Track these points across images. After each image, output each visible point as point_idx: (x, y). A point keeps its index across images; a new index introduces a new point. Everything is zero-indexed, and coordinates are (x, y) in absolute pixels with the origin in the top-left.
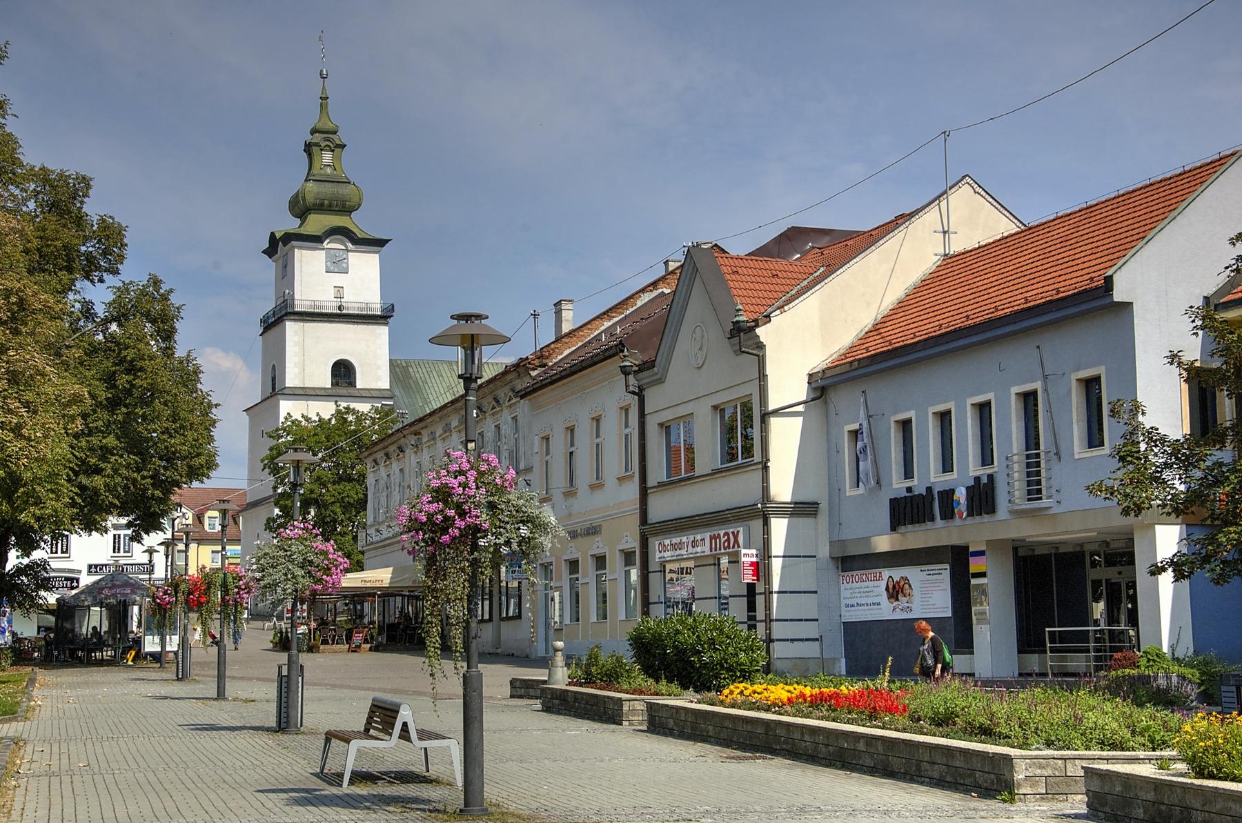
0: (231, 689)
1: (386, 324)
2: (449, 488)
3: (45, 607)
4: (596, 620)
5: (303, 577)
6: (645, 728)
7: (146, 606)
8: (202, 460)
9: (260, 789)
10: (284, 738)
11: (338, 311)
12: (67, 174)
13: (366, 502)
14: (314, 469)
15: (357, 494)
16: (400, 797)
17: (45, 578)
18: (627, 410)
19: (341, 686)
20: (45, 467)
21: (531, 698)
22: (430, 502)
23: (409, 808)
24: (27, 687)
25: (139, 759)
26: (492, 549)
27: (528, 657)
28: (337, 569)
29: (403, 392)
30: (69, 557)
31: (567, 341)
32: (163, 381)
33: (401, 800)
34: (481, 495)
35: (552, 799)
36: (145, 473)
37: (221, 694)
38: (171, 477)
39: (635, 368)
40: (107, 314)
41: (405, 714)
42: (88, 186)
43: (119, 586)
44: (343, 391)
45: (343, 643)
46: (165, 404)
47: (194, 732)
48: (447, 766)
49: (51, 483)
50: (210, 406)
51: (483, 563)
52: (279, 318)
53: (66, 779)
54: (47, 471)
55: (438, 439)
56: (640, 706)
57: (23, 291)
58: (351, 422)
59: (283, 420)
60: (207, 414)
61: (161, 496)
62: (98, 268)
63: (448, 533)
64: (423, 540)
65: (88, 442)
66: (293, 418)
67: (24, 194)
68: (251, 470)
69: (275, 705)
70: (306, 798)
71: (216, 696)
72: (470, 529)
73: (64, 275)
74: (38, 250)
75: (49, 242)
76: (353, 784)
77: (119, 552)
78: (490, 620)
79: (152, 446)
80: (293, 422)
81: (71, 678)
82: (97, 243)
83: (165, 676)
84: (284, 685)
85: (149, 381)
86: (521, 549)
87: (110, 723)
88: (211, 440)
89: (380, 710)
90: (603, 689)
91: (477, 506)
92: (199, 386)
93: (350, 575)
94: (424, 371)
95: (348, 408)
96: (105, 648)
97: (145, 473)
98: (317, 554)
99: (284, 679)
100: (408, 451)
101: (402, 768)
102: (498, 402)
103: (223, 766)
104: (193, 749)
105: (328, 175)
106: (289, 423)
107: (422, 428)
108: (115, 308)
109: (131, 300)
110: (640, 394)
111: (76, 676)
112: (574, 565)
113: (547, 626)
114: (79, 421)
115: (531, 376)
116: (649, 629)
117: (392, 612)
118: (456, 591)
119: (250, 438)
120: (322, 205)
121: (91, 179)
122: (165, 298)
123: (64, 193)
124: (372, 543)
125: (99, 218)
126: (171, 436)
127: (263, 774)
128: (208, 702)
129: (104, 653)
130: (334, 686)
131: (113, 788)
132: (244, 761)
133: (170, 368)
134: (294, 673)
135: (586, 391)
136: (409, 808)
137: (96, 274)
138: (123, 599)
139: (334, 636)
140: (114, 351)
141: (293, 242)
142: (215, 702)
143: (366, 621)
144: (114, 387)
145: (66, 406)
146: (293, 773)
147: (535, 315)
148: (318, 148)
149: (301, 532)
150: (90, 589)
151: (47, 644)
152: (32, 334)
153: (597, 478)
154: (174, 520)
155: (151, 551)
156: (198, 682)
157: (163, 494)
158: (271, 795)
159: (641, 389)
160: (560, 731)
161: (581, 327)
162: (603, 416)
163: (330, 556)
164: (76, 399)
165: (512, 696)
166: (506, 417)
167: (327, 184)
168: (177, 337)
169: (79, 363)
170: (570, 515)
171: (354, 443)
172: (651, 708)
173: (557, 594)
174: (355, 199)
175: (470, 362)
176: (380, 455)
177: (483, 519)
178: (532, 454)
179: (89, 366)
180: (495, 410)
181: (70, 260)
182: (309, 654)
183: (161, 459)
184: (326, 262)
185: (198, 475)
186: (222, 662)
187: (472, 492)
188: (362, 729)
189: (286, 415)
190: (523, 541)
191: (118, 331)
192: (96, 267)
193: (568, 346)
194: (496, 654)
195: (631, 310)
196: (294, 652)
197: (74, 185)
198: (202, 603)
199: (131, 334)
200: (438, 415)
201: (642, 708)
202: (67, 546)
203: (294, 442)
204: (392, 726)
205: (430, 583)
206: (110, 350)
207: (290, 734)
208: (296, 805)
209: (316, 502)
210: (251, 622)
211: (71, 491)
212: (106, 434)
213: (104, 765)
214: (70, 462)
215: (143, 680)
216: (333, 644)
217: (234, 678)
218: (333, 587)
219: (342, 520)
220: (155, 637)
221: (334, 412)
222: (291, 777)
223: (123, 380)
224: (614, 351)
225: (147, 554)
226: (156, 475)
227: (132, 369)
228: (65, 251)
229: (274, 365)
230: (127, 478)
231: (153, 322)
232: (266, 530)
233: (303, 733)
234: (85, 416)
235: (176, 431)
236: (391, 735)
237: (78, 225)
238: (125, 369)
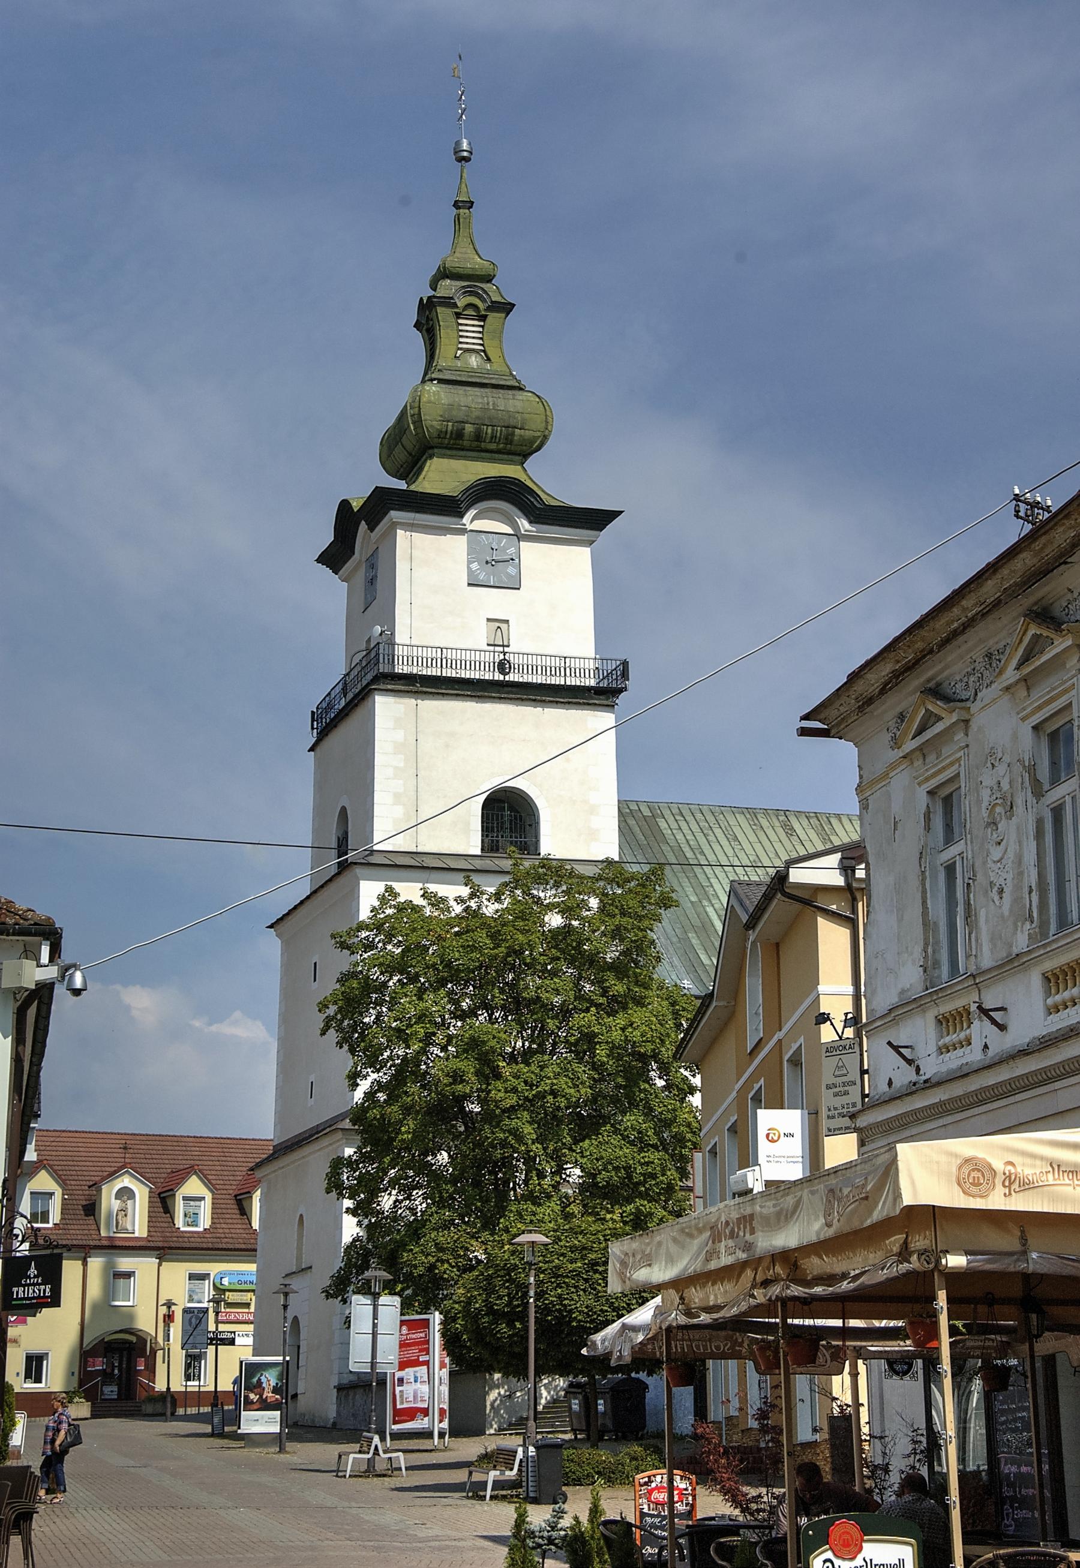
1: (610, 707)
9: (485, 1534)
66: (401, 899)
80: (401, 908)
94: (694, 827)
106: (390, 911)
120: (459, 434)
141: (393, 513)
174: (536, 424)
184: (469, 562)
210: (290, 1446)
229: (344, 810)
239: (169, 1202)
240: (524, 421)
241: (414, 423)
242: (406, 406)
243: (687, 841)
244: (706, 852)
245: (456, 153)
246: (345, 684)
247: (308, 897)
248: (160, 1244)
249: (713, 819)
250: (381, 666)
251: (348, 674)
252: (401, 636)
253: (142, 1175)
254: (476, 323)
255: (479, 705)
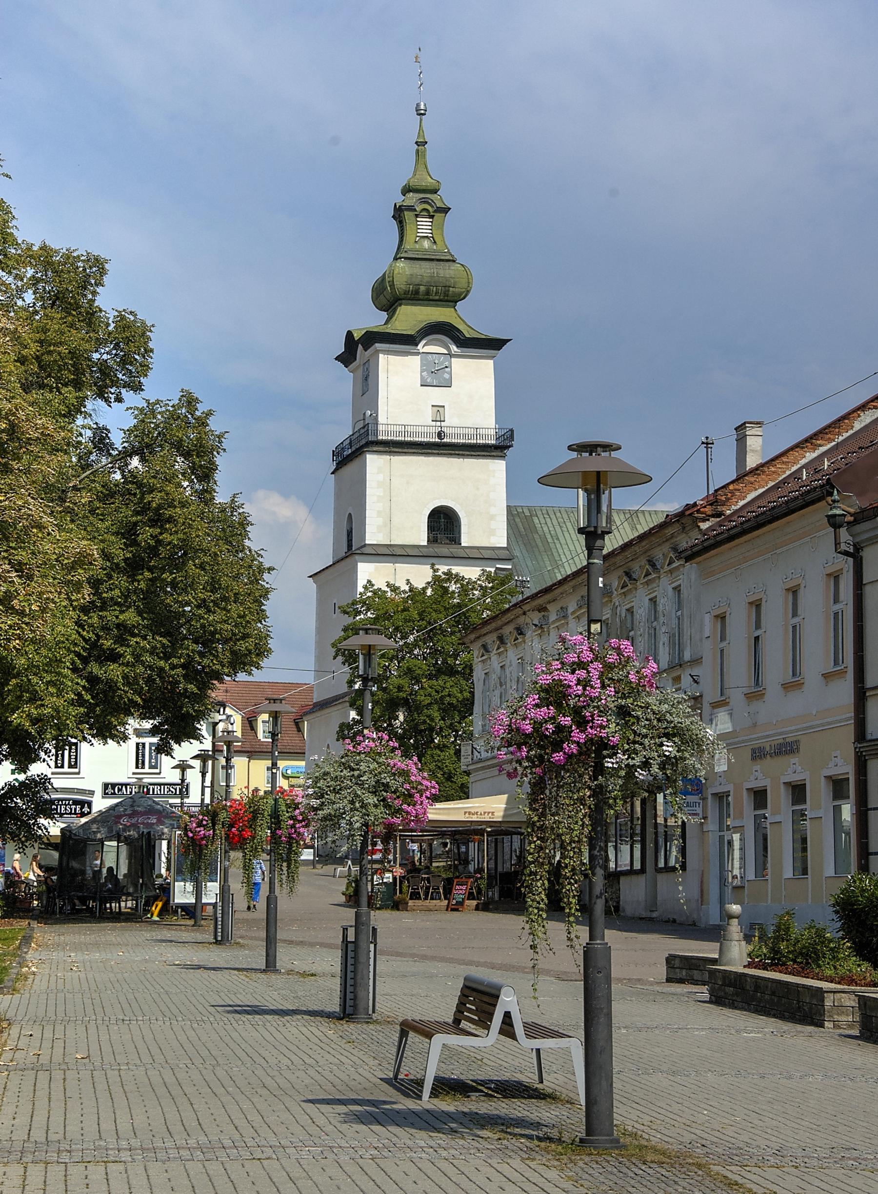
0: (284, 957)
1: (502, 457)
2: (563, 686)
3: (45, 840)
4: (791, 876)
5: (376, 806)
6: (856, 1032)
7: (176, 840)
8: (250, 644)
9: (310, 1098)
10: (350, 1028)
11: (437, 440)
12: (75, 254)
13: (473, 703)
14: (403, 658)
15: (461, 692)
16: (499, 1117)
17: (46, 800)
18: (837, 578)
19: (433, 958)
20: (44, 652)
21: (696, 983)
22: (537, 706)
23: (510, 1134)
24: (19, 948)
25: (155, 1050)
26: (623, 773)
27: (694, 924)
28: (421, 796)
29: (524, 551)
30: (79, 773)
31: (752, 479)
32: (198, 536)
33: (500, 1121)
34: (609, 697)
35: (713, 1130)
36: (175, 661)
37: (271, 965)
38: (209, 666)
39: (849, 518)
40: (126, 445)
41: (508, 1001)
42: (103, 272)
43: (142, 814)
44: (444, 550)
45: (440, 899)
46: (202, 567)
47: (230, 1016)
48: (569, 1076)
49: (51, 672)
50: (261, 570)
51: (610, 792)
52: (357, 450)
53: (58, 1075)
54: (45, 657)
55: (571, 617)
56: (850, 1001)
57: (14, 414)
58: (453, 592)
59: (362, 590)
60: (257, 580)
61: (195, 690)
62: (115, 383)
63: (562, 749)
64: (528, 758)
65: (101, 618)
66: (375, 587)
67: (20, 283)
68: (319, 658)
69: (338, 981)
70: (370, 1114)
71: (264, 967)
72: (592, 744)
73: (70, 393)
74: (37, 358)
75: (52, 348)
76: (436, 1096)
77: (143, 768)
78: (643, 870)
79: (185, 623)
80: (375, 593)
81: (77, 936)
82: (114, 348)
83: (199, 937)
84: (351, 954)
85: (181, 536)
86: (666, 774)
87: (122, 999)
88: (261, 615)
89: (475, 994)
90: (798, 974)
91: (603, 712)
92: (247, 543)
93: (438, 805)
94: (555, 522)
95: (449, 574)
96: (124, 898)
97: (175, 661)
98: (394, 774)
99: (351, 947)
100: (529, 634)
101: (506, 1076)
102: (653, 565)
103: (265, 1064)
104: (227, 1039)
105: (426, 250)
106: (369, 594)
107: (549, 602)
108: (136, 436)
109: (157, 426)
110: (856, 555)
111: (85, 934)
112: (760, 797)
113: (723, 881)
114: (87, 590)
115: (701, 530)
116: (863, 890)
117: (507, 857)
118: (573, 830)
119: (319, 614)
120: (417, 292)
121: (106, 261)
122: (202, 422)
123: (71, 281)
124: (480, 761)
125: (117, 314)
126: (209, 611)
127: (318, 1077)
128: (253, 975)
129: (123, 904)
130: (424, 958)
131: (116, 1089)
132: (293, 1057)
133: (208, 518)
134: (363, 937)
135: (778, 551)
136: (510, 1134)
137: (112, 391)
138: (146, 831)
139: (428, 888)
140: (135, 494)
141: (377, 345)
142: (263, 976)
143: (471, 868)
144: (135, 543)
145: (72, 567)
146: (357, 1077)
147: (707, 444)
148: (412, 214)
149: (372, 744)
150: (106, 816)
151: (49, 889)
152: (27, 472)
153: (794, 674)
154: (215, 724)
155: (183, 767)
156: (242, 946)
157: (199, 689)
158: (325, 1108)
159: (858, 548)
160: (733, 1031)
161: (773, 460)
162: (802, 586)
163: (413, 778)
164: (82, 560)
165: (669, 980)
166: (664, 587)
167: (423, 263)
168: (218, 476)
169: (90, 512)
170: (755, 725)
171: (458, 623)
172: (865, 1004)
173: (736, 837)
174: (462, 284)
175: (594, 512)
176: (491, 639)
177: (612, 730)
178: (701, 640)
179: (102, 515)
180: (650, 577)
181: (78, 371)
182: (393, 912)
183: (196, 641)
184: (421, 372)
185: (245, 664)
186: (272, 921)
187: (595, 693)
188: (450, 1020)
189: (365, 582)
190: (667, 762)
191: (140, 467)
192: (112, 381)
193: (753, 487)
194: (651, 919)
195: (846, 435)
196: (364, 909)
197: (84, 270)
198: (245, 839)
199: (157, 472)
200: (572, 584)
201: (853, 1004)
202: (76, 758)
203: (376, 620)
204: (490, 1015)
205: (536, 819)
206: (130, 494)
207: (358, 1023)
208: (357, 1123)
209: (406, 703)
211: (77, 684)
212: (123, 607)
213: (108, 1058)
214: (76, 644)
215: (171, 941)
216: (426, 899)
217: (291, 942)
218: (418, 820)
219: (441, 728)
220: (188, 884)
221: (430, 580)
222: (353, 1083)
223: (146, 534)
224: (818, 493)
225: (178, 770)
226: (190, 663)
227: (158, 520)
228: (72, 359)
229: (350, 515)
230: (151, 668)
231: (187, 455)
232: (338, 740)
233: (376, 1022)
234: (95, 584)
235: (216, 604)
236: (488, 1028)
237: (89, 324)
238: (149, 520)
239: (254, 723)
240: (455, 283)
241: (390, 286)
242: (384, 274)
243: (550, 531)
244: (560, 539)
245: (417, 111)
246: (351, 441)
247: (330, 566)
248: (249, 750)
249: (566, 516)
250: (370, 437)
251: (353, 435)
252: (382, 419)
253: (239, 709)
254: (428, 220)
255: (426, 458)
